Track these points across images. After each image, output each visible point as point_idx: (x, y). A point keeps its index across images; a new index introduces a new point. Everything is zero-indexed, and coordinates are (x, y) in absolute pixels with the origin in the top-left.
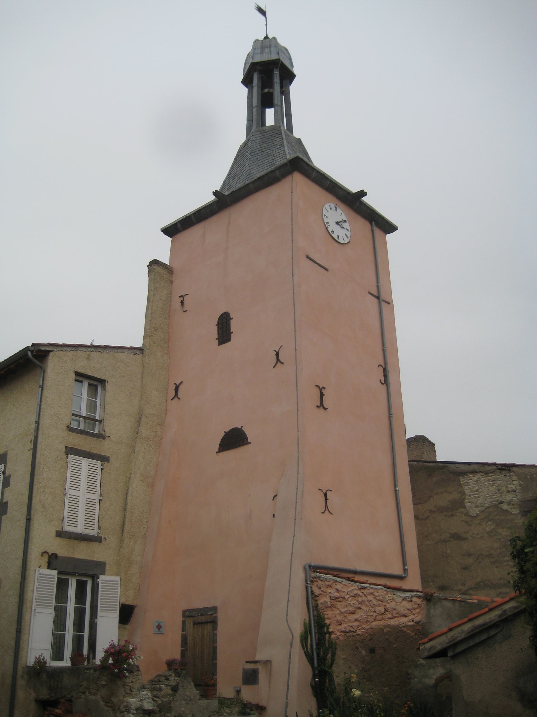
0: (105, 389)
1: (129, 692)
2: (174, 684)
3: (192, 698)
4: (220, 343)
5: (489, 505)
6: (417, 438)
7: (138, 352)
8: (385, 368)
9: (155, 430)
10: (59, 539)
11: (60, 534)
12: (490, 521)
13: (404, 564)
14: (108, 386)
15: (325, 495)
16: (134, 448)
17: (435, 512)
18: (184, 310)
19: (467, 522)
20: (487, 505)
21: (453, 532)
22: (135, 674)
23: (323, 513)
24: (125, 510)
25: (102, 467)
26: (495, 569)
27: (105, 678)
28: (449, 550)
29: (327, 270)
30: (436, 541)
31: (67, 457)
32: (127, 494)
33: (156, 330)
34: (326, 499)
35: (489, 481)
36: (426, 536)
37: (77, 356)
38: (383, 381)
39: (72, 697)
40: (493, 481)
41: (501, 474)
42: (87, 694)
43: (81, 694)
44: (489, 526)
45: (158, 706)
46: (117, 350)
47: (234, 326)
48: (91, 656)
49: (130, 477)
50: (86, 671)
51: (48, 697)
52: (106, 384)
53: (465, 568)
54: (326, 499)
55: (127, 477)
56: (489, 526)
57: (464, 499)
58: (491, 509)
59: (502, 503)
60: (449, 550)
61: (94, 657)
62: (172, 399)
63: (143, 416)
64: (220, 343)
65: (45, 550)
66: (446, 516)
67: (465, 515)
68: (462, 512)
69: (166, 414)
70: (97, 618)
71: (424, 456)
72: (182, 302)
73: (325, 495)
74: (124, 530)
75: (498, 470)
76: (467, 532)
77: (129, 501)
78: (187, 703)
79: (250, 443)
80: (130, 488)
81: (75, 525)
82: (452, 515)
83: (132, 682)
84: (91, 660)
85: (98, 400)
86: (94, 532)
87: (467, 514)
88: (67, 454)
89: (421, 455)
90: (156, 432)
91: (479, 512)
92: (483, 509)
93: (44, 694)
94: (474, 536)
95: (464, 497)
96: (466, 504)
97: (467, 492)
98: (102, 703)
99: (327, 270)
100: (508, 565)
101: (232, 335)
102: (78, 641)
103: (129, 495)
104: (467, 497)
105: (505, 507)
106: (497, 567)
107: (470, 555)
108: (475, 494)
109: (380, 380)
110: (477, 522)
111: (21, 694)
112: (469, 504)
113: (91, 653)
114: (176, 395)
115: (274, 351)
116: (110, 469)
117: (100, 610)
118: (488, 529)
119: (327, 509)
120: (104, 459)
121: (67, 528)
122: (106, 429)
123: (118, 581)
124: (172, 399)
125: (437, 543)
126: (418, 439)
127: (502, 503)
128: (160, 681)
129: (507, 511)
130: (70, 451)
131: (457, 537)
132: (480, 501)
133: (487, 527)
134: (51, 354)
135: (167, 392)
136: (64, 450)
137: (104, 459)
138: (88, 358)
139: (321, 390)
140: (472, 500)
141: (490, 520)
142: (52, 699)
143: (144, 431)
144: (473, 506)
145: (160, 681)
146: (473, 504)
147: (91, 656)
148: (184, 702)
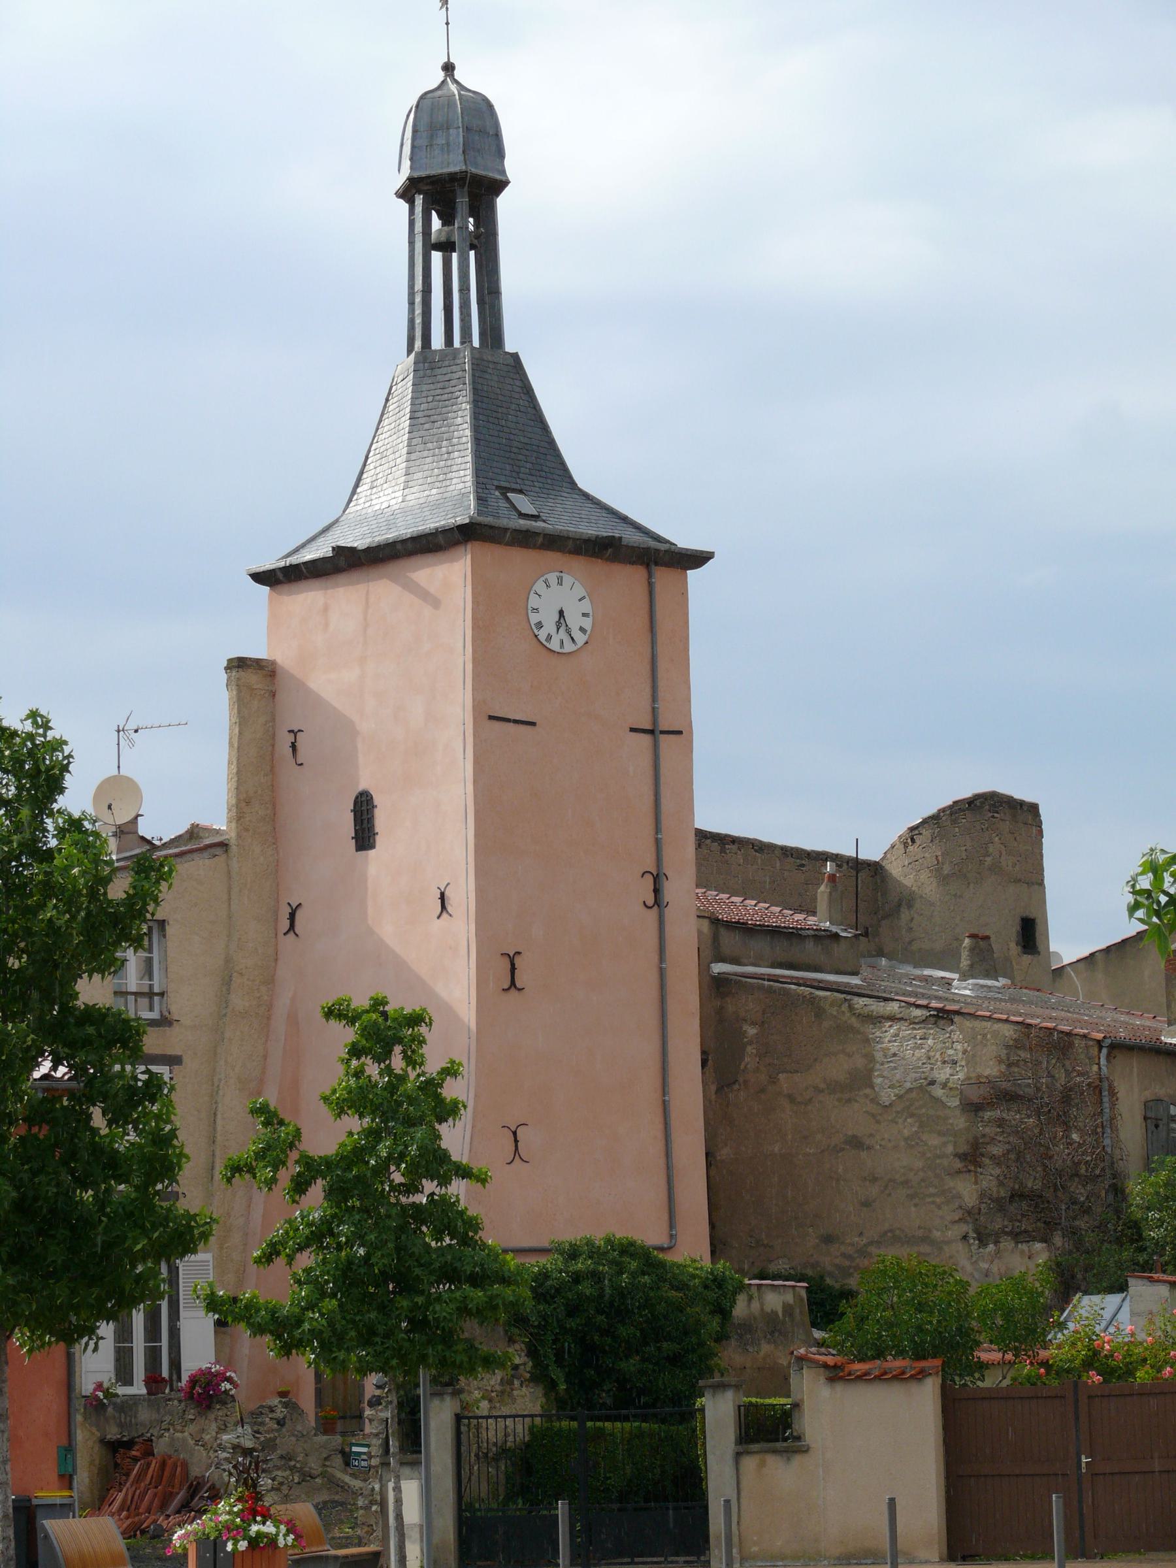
0: (164, 936)
1: (223, 1427)
2: (281, 1416)
3: (305, 1433)
5: (912, 1086)
6: (976, 800)
7: (218, 851)
8: (657, 875)
9: (258, 995)
12: (911, 1117)
13: (672, 1224)
14: (169, 930)
15: (515, 1133)
16: (222, 1033)
17: (822, 1091)
18: (299, 762)
19: (873, 1116)
20: (908, 1085)
21: (850, 1133)
22: (229, 1406)
23: (509, 1163)
24: (214, 1142)
25: (170, 1076)
26: (913, 1209)
27: (192, 1411)
28: (841, 1167)
29: (533, 724)
30: (822, 1148)
32: (215, 1114)
33: (248, 803)
34: (516, 1141)
35: (915, 1037)
36: (806, 1138)
38: (650, 902)
39: (152, 1435)
41: (938, 1027)
42: (171, 1430)
43: (163, 1432)
44: (908, 1127)
45: (261, 1443)
46: (180, 860)
47: (381, 820)
48: (175, 1377)
49: (218, 1086)
50: (168, 1402)
51: (119, 1436)
52: (167, 927)
53: (866, 1204)
54: (516, 1141)
55: (213, 1085)
56: (908, 1127)
57: (872, 1070)
58: (914, 1095)
59: (932, 1083)
60: (841, 1167)
61: (179, 1379)
62: (285, 934)
63: (235, 974)
66: (839, 1100)
67: (872, 1101)
68: (867, 1096)
69: (276, 960)
70: (179, 1320)
71: (991, 850)
72: (294, 746)
73: (515, 1133)
74: (214, 1177)
75: (931, 1019)
76: (871, 1135)
77: (219, 1128)
78: (297, 1440)
80: (220, 1105)
82: (849, 1101)
83: (227, 1415)
84: (175, 1383)
85: (155, 955)
87: (875, 1100)
89: (984, 846)
90: (259, 998)
91: (894, 1098)
92: (902, 1092)
93: (113, 1433)
94: (883, 1143)
95: (872, 1065)
96: (875, 1080)
97: (879, 1056)
98: (192, 1442)
99: (533, 724)
100: (933, 1203)
101: (377, 838)
102: (153, 1356)
103: (219, 1116)
104: (878, 1066)
105: (938, 1092)
106: (916, 1205)
107: (874, 1179)
108: (891, 1062)
109: (644, 902)
110: (890, 1118)
111: (80, 1435)
112: (880, 1080)
113: (174, 1372)
114: (292, 926)
115: (439, 888)
117: (184, 1307)
118: (906, 1132)
119: (517, 1154)
122: (173, 1009)
123: (209, 1261)
124: (285, 934)
125: (823, 1151)
126: (978, 804)
127: (933, 1085)
128: (262, 1414)
129: (937, 1100)
131: (856, 1143)
132: (898, 1077)
135: (277, 919)
140: (885, 1073)
141: (912, 1115)
142: (125, 1439)
143: (239, 1001)
144: (886, 1084)
145: (262, 1414)
146: (886, 1081)
147: (175, 1377)
148: (293, 1439)
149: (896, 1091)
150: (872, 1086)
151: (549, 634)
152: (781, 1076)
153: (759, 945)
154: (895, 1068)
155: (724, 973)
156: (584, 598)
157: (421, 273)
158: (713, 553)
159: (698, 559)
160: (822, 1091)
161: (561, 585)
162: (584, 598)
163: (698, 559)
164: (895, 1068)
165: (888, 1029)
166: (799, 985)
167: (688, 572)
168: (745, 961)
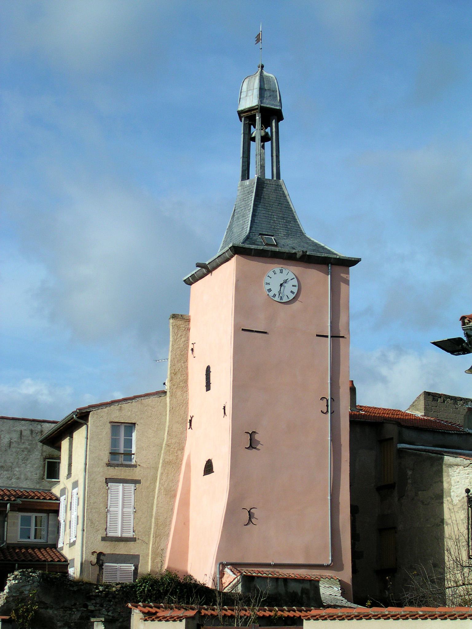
4: (207, 391)
10: (103, 542)
11: (105, 539)
23: (246, 525)
31: (107, 486)
37: (111, 410)
40: (468, 474)
64: (207, 391)
65: (94, 551)
79: (214, 472)
81: (116, 531)
86: (130, 535)
88: (107, 483)
114: (190, 425)
116: (142, 489)
120: (136, 482)
121: (110, 534)
130: (108, 481)
133: (461, 515)
134: (91, 413)
136: (104, 481)
137: (136, 482)
138: (121, 409)
139: (251, 435)
149: (459, 498)
150: (450, 496)
151: (275, 294)
152: (419, 493)
153: (427, 437)
154: (458, 488)
155: (403, 448)
156: (294, 278)
157: (275, 160)
158: (360, 259)
159: (354, 262)
160: (433, 499)
161: (282, 273)
162: (294, 278)
163: (354, 262)
164: (458, 488)
165: (456, 470)
166: (432, 453)
167: (350, 268)
168: (419, 444)
